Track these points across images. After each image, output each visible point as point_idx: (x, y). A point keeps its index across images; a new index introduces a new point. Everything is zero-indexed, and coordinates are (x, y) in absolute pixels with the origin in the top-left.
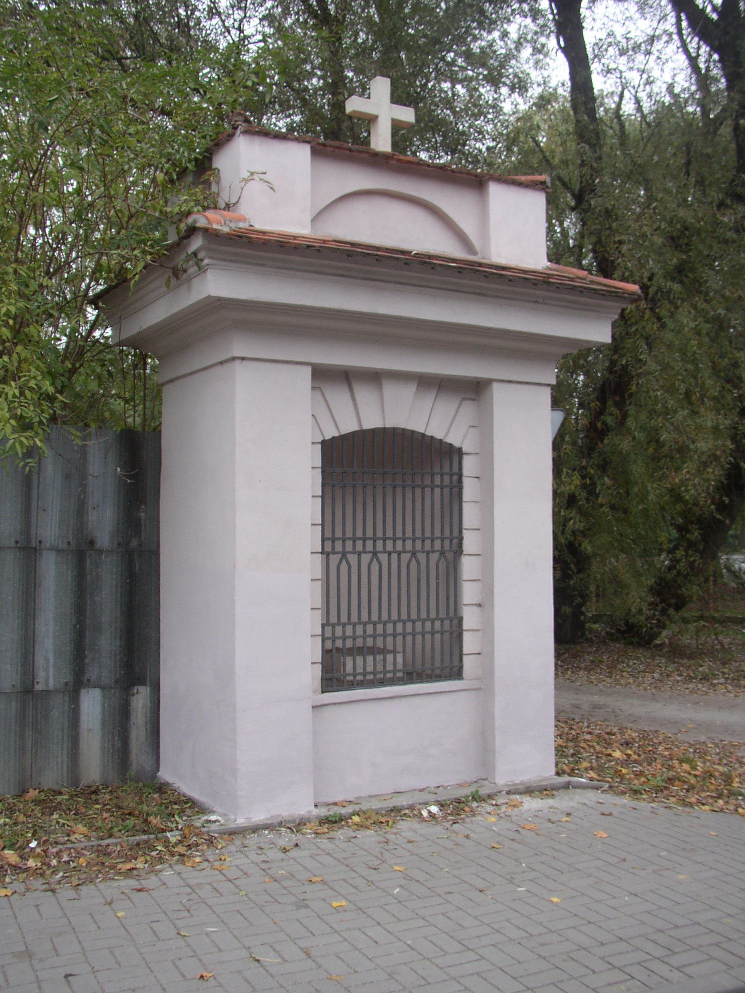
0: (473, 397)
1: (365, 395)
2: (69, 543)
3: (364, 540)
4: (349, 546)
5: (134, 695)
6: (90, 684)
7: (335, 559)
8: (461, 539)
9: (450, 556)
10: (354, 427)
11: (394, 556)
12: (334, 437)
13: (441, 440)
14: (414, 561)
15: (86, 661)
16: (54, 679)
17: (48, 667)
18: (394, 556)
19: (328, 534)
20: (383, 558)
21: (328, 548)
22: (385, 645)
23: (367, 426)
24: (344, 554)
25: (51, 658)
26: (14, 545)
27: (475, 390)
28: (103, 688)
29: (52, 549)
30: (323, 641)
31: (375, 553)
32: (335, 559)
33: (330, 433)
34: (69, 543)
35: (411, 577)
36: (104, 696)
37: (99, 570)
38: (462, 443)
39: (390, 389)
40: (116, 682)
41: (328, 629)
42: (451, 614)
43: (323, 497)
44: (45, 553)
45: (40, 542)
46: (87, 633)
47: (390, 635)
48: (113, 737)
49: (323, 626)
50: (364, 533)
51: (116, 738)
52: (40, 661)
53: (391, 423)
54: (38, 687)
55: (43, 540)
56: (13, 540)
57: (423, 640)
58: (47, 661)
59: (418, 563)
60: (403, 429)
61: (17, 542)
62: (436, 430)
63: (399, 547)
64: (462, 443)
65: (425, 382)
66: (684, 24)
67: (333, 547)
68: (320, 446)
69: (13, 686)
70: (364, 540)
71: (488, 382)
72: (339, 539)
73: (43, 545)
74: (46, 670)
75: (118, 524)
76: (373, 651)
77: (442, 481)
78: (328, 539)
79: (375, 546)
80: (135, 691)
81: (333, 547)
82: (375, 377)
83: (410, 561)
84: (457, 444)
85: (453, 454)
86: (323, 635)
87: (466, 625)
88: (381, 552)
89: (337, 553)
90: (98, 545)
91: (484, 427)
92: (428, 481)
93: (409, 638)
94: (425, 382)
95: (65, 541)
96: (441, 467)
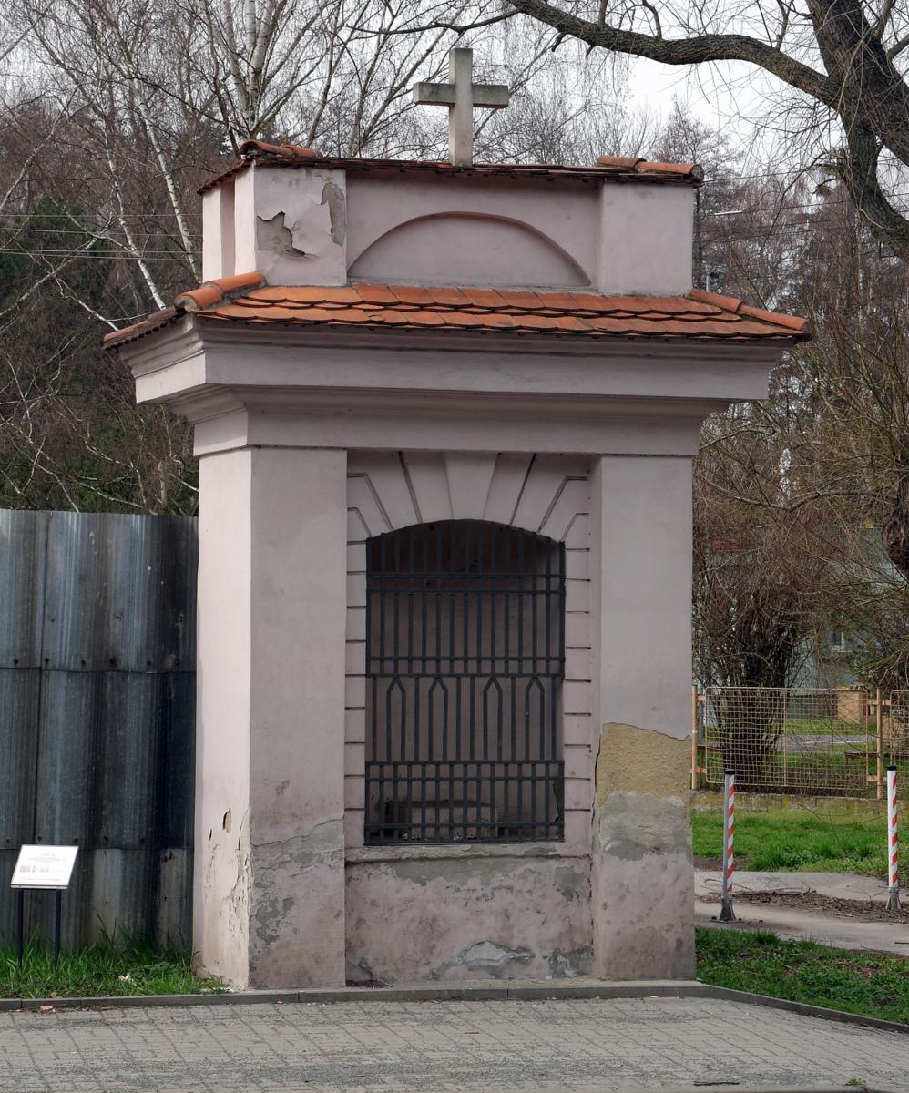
1: (424, 481)
2: (83, 663)
4: (500, 667)
5: (166, 860)
6: (107, 844)
8: (562, 660)
10: (413, 521)
11: (466, 682)
12: (383, 534)
14: (396, 690)
15: (104, 813)
16: (61, 834)
17: (54, 819)
18: (466, 682)
19: (376, 653)
21: (375, 669)
22: (465, 795)
23: (429, 517)
24: (438, 677)
25: (58, 808)
26: (12, 665)
28: (124, 849)
29: (63, 671)
30: (367, 783)
31: (438, 677)
33: (378, 529)
34: (83, 663)
35: (517, 707)
36: (125, 860)
38: (565, 535)
39: (456, 473)
40: (142, 841)
42: (548, 757)
43: (368, 608)
44: (53, 674)
45: (47, 660)
46: (106, 777)
49: (368, 765)
50: (507, 651)
51: (139, 915)
52: (43, 811)
53: (460, 514)
55: (50, 658)
56: (11, 659)
58: (53, 812)
61: (16, 662)
62: (528, 520)
64: (565, 535)
65: (502, 460)
67: (479, 668)
68: (364, 546)
69: (8, 841)
73: (50, 664)
74: (51, 823)
75: (148, 638)
78: (375, 659)
80: (168, 854)
81: (479, 668)
82: (437, 460)
84: (557, 538)
86: (367, 775)
88: (543, 675)
89: (485, 675)
90: (122, 665)
92: (542, 585)
94: (502, 460)
95: (79, 661)
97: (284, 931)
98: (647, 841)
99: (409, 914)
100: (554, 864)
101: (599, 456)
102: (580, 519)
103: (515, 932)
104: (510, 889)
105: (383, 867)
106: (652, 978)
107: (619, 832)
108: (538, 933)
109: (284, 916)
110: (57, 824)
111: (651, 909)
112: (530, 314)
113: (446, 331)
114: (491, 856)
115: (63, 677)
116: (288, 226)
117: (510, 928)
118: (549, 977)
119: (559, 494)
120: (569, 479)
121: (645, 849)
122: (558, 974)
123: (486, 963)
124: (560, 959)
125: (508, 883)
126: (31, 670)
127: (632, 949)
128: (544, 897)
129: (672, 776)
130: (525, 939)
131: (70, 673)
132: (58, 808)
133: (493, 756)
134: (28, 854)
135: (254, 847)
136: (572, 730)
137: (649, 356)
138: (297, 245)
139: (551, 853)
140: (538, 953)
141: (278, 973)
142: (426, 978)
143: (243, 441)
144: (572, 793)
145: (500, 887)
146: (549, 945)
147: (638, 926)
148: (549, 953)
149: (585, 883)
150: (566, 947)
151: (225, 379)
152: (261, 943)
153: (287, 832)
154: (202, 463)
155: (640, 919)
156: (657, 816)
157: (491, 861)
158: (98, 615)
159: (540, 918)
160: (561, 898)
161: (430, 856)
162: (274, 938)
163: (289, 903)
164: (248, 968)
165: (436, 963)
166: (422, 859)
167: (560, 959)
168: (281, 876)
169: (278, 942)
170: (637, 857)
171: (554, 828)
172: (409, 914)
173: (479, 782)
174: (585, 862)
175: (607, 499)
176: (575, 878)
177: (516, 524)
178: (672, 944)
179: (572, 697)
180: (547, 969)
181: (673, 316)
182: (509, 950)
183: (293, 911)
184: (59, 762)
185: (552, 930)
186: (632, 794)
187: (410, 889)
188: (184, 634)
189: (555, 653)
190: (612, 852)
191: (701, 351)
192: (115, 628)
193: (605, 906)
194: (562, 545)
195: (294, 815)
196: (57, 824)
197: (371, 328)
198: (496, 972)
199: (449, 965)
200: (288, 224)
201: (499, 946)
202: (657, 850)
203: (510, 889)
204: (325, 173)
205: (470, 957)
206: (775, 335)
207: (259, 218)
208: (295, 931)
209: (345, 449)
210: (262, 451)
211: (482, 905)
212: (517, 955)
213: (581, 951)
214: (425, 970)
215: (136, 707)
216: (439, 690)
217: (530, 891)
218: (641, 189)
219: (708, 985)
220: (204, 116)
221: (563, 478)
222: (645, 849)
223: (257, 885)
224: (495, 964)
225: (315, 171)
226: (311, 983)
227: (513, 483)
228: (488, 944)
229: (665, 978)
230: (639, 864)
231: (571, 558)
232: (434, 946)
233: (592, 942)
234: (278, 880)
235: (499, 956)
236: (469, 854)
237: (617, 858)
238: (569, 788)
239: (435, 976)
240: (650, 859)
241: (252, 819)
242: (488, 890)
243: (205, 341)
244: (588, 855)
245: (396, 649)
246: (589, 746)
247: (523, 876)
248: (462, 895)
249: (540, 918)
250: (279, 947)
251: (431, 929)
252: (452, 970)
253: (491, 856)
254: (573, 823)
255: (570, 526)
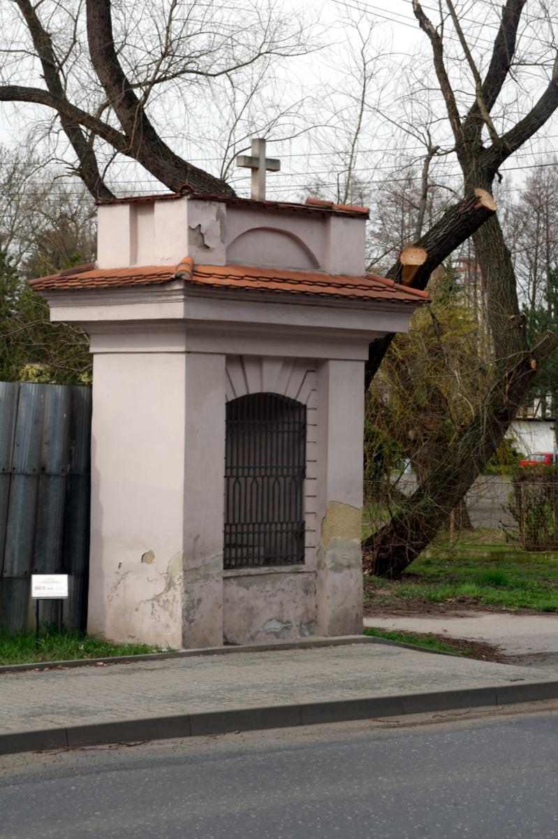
0: (313, 369)
1: (252, 371)
2: (34, 470)
3: (237, 468)
7: (232, 480)
8: (305, 468)
9: (297, 478)
13: (294, 400)
18: (266, 479)
20: (259, 479)
25: (16, 553)
27: (315, 365)
32: (232, 480)
37: (47, 489)
39: (267, 367)
41: (228, 527)
42: (298, 519)
47: (251, 533)
48: (52, 611)
54: (5, 575)
55: (16, 467)
57: (254, 537)
59: (257, 483)
60: (277, 394)
62: (291, 394)
63: (263, 474)
64: (307, 401)
66: (540, 407)
70: (237, 468)
71: (326, 360)
72: (235, 467)
73: (15, 471)
74: (12, 562)
76: (241, 546)
77: (289, 428)
79: (255, 472)
82: (259, 360)
83: (252, 484)
84: (303, 402)
85: (298, 409)
87: (307, 526)
90: (48, 471)
91: (322, 390)
93: (251, 535)
96: (289, 419)
97: (197, 617)
98: (345, 563)
99: (242, 605)
100: (300, 576)
101: (327, 360)
102: (313, 392)
103: (285, 613)
104: (283, 590)
105: (232, 580)
106: (346, 634)
107: (334, 558)
108: (294, 613)
109: (197, 609)
110: (16, 563)
111: (346, 598)
112: (370, 289)
113: (293, 294)
114: (277, 573)
115: (22, 479)
116: (203, 232)
117: (283, 611)
118: (299, 637)
119: (305, 376)
120: (308, 371)
121: (344, 567)
122: (302, 635)
123: (273, 630)
124: (303, 626)
125: (282, 587)
126: (10, 474)
127: (338, 620)
128: (296, 594)
129: (355, 528)
130: (289, 616)
131: (27, 475)
132: (16, 553)
133: (276, 520)
134: (37, 580)
135: (185, 571)
136: (309, 505)
137: (364, 309)
138: (207, 243)
139: (301, 571)
140: (294, 623)
141: (194, 640)
142: (249, 640)
143: (183, 349)
144: (309, 538)
145: (279, 590)
146: (298, 619)
147: (342, 607)
148: (298, 623)
149: (313, 586)
150: (305, 620)
151: (192, 317)
152: (187, 624)
153: (199, 563)
154: (95, 357)
155: (342, 604)
156: (349, 549)
157: (275, 575)
158: (39, 441)
159: (295, 605)
160: (304, 594)
161: (252, 574)
162: (192, 621)
163: (199, 601)
164: (181, 638)
165: (253, 632)
166: (249, 576)
167: (303, 626)
168: (196, 586)
169: (195, 623)
170: (341, 571)
171: (302, 559)
172: (242, 605)
173: (270, 533)
174: (313, 575)
175: (332, 385)
176: (308, 584)
177: (264, 391)
178: (354, 617)
179: (309, 487)
180: (297, 632)
181: (356, 287)
182: (282, 623)
183: (201, 606)
184: (18, 527)
185: (300, 611)
186: (339, 538)
187: (242, 592)
188: (75, 452)
189: (302, 464)
190: (331, 569)
191: (386, 307)
192: (46, 449)
193: (328, 597)
194: (305, 406)
195: (201, 554)
196: (16, 563)
197: (262, 291)
198: (277, 635)
199: (258, 632)
200: (202, 231)
201: (279, 621)
202: (349, 567)
203: (283, 590)
204: (217, 204)
205: (266, 628)
206: (420, 300)
207: (190, 227)
208: (202, 616)
209: (225, 354)
210: (190, 355)
211: (272, 599)
212: (286, 625)
213: (311, 622)
214: (248, 635)
215: (55, 492)
216: (277, 483)
217: (291, 591)
218: (345, 220)
219: (372, 637)
220: (503, 209)
221: (305, 371)
222: (344, 567)
223: (186, 592)
224: (276, 631)
225: (213, 203)
226: (209, 645)
227: (298, 376)
228: (274, 620)
229: (351, 634)
230: (342, 574)
231: (310, 414)
232: (252, 623)
233: (316, 617)
234: (195, 589)
235: (277, 626)
236: (267, 572)
237: (333, 572)
238: (308, 536)
239: (252, 638)
240: (346, 571)
241: (184, 555)
242: (274, 591)
243: (185, 295)
244: (315, 571)
245: (238, 464)
246: (315, 513)
247: (288, 583)
248: (263, 594)
249: (295, 605)
250: (195, 625)
251: (251, 612)
252: (259, 635)
253: (277, 573)
254: (309, 554)
255: (309, 397)
